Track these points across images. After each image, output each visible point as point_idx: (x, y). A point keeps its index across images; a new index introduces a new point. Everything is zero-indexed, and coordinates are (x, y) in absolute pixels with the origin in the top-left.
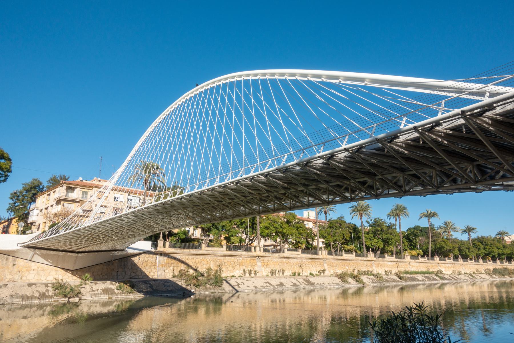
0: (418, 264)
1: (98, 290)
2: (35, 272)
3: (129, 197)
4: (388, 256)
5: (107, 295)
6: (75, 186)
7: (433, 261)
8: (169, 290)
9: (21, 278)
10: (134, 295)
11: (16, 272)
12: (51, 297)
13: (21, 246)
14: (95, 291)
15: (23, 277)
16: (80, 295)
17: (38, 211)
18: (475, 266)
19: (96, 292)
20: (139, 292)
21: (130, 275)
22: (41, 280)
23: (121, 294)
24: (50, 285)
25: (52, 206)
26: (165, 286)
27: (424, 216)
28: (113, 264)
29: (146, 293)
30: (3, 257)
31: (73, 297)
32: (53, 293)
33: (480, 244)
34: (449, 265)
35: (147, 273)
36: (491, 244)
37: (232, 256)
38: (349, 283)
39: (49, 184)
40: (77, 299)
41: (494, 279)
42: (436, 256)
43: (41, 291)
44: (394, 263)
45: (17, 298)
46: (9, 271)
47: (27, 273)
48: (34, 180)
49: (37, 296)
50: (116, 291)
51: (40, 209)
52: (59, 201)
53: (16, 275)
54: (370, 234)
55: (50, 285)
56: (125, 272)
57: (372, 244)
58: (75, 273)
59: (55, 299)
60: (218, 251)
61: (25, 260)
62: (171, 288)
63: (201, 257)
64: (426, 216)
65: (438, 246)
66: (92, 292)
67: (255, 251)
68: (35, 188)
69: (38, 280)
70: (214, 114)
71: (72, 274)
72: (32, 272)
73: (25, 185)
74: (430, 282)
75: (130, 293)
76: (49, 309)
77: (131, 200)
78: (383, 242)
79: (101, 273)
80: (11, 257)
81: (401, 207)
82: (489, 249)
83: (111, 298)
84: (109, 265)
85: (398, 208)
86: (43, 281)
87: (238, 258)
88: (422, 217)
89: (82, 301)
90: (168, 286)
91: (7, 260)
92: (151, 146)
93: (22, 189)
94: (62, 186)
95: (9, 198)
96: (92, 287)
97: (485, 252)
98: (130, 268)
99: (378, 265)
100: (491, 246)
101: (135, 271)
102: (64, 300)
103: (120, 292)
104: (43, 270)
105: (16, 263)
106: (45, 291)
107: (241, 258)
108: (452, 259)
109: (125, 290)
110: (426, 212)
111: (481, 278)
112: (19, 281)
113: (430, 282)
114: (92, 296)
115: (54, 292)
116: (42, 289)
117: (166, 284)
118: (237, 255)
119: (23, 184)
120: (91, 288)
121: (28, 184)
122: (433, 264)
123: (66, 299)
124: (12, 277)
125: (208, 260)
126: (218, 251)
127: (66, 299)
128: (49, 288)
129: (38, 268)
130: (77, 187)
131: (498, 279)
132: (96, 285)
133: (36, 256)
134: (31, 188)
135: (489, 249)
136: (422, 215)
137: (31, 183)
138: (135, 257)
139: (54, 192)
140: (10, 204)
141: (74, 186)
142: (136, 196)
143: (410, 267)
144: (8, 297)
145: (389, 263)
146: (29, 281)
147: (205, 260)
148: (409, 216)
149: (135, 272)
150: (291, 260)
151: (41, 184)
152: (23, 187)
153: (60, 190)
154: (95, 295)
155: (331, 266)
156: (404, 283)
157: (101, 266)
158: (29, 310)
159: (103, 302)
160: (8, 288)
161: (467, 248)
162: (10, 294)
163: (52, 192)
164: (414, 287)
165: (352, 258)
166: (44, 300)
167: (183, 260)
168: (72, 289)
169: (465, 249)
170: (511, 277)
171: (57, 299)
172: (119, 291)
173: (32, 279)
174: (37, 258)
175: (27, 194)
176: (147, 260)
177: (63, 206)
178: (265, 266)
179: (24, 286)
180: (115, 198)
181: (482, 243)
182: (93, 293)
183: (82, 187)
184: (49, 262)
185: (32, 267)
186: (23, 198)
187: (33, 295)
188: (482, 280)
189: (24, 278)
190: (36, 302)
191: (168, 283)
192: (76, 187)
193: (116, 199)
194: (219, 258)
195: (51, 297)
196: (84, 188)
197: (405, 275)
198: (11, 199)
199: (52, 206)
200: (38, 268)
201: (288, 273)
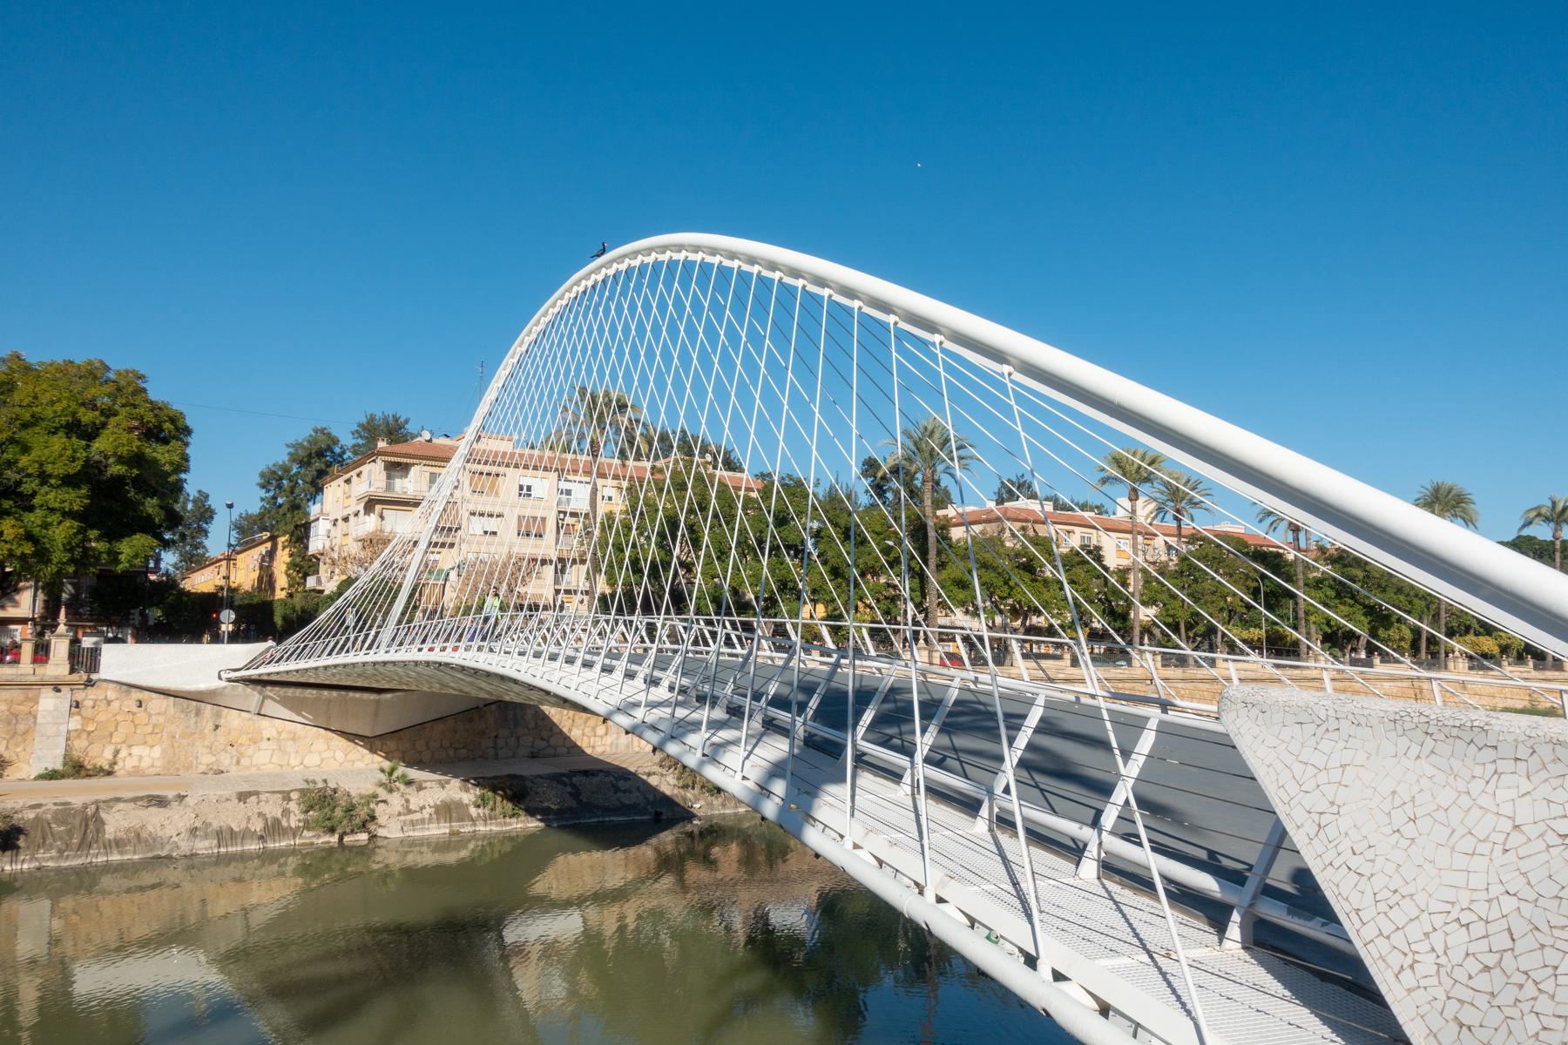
1: (422, 808)
2: (272, 745)
3: (564, 485)
4: (1382, 662)
5: (448, 825)
6: (408, 461)
7: (1557, 673)
8: (628, 806)
9: (238, 762)
10: (522, 822)
11: (222, 747)
12: (295, 832)
13: (229, 680)
14: (416, 812)
15: (242, 761)
16: (372, 827)
17: (328, 525)
19: (417, 816)
21: (532, 746)
22: (288, 764)
23: (485, 820)
24: (295, 796)
25: (356, 515)
26: (617, 790)
27: (1537, 520)
28: (481, 717)
30: (188, 707)
31: (352, 832)
32: (300, 821)
39: (360, 441)
40: (363, 837)
43: (268, 816)
44: (1406, 684)
45: (206, 837)
46: (207, 743)
47: (253, 747)
48: (316, 431)
49: (258, 830)
50: (473, 811)
51: (332, 518)
52: (371, 504)
53: (223, 753)
54: (1325, 589)
55: (295, 796)
56: (518, 739)
58: (378, 743)
59: (305, 838)
61: (243, 713)
62: (635, 797)
64: (1547, 519)
66: (405, 815)
68: (320, 454)
69: (282, 766)
70: (620, 353)
72: (264, 745)
73: (294, 446)
75: (512, 816)
76: (292, 862)
77: (568, 492)
78: (1371, 615)
79: (451, 744)
80: (209, 706)
81: (1449, 492)
83: (458, 833)
84: (471, 721)
85: (1437, 498)
86: (293, 767)
88: (1530, 523)
89: (380, 842)
90: (625, 792)
91: (197, 714)
92: (528, 393)
93: (286, 458)
94: (374, 461)
95: (258, 484)
96: (407, 801)
98: (532, 726)
101: (545, 734)
102: (328, 842)
103: (484, 814)
104: (293, 739)
105: (222, 721)
106: (279, 816)
109: (499, 810)
110: (1550, 504)
112: (234, 768)
114: (405, 828)
115: (302, 817)
116: (273, 809)
117: (622, 784)
119: (287, 446)
120: (403, 802)
121: (301, 445)
123: (334, 839)
124: (214, 759)
127: (334, 839)
128: (293, 806)
129: (280, 733)
130: (415, 461)
132: (421, 793)
133: (268, 702)
134: (310, 455)
136: (1534, 513)
137: (309, 442)
139: (358, 475)
140: (262, 500)
141: (405, 460)
142: (578, 478)
144: (183, 835)
146: (258, 769)
148: (1477, 525)
149: (545, 737)
151: (336, 441)
152: (290, 454)
153: (370, 471)
154: (413, 823)
157: (451, 721)
158: (241, 866)
159: (437, 843)
160: (186, 806)
162: (188, 826)
163: (354, 473)
166: (274, 841)
168: (350, 809)
171: (311, 837)
172: (480, 811)
173: (265, 765)
174: (271, 707)
175: (303, 471)
177: (382, 517)
179: (227, 800)
180: (521, 488)
182: (409, 817)
183: (427, 462)
185: (264, 732)
186: (292, 484)
187: (247, 827)
189: (245, 762)
190: (253, 846)
191: (626, 779)
192: (412, 461)
193: (525, 491)
195: (295, 832)
196: (434, 463)
198: (263, 487)
199: (356, 515)
200: (280, 733)
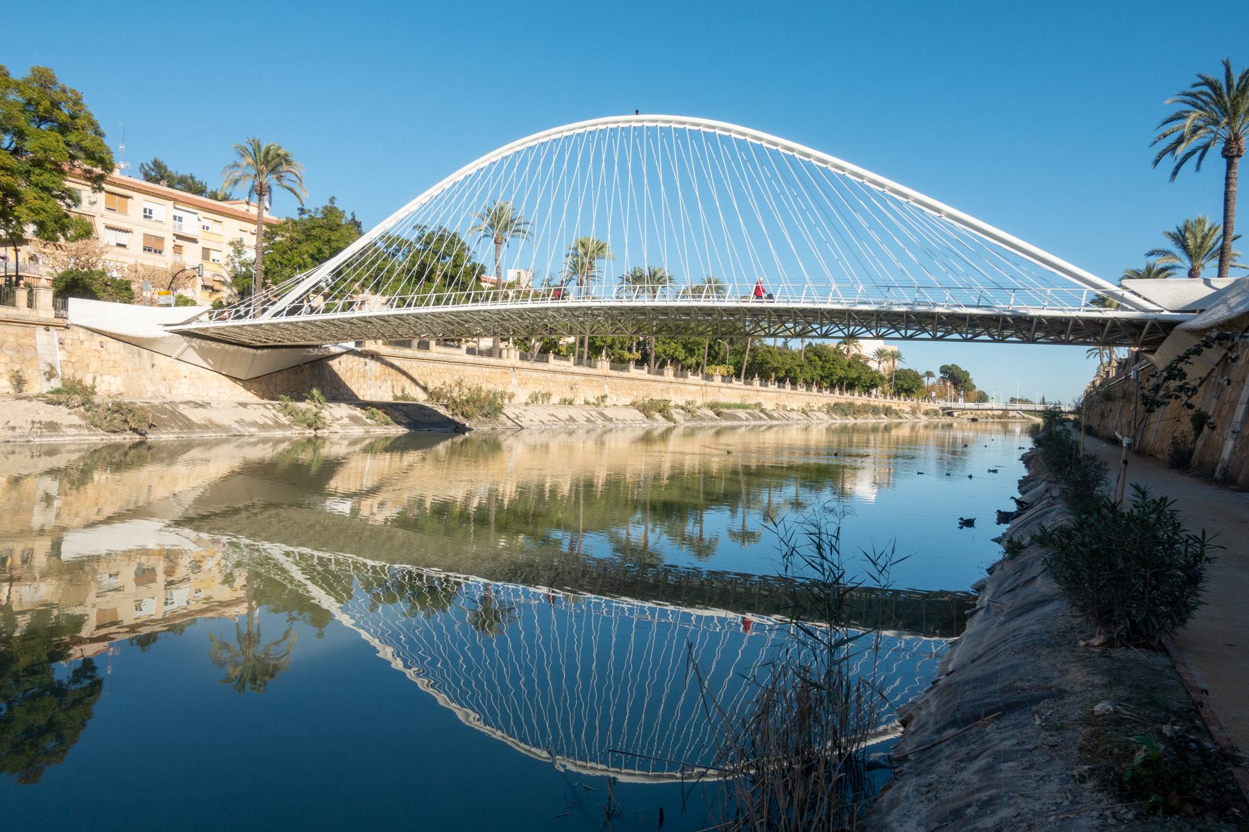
0: (730, 391)
9: (170, 392)
18: (803, 397)
20: (399, 423)
29: (407, 425)
33: (817, 358)
34: (772, 394)
35: (355, 391)
36: (834, 361)
37: (748, 390)
38: (657, 420)
41: (834, 421)
42: (604, 358)
44: (699, 388)
46: (149, 377)
57: (665, 351)
60: (450, 354)
63: (431, 365)
65: (759, 359)
67: (31, 304)
71: (245, 388)
74: (756, 423)
82: (830, 368)
87: (484, 369)
97: (821, 373)
99: (676, 391)
100: (833, 364)
101: (337, 386)
105: (155, 362)
107: (487, 370)
108: (572, 359)
111: (818, 419)
113: (756, 423)
118: (483, 363)
122: (750, 392)
125: (441, 371)
126: (450, 354)
131: (838, 421)
135: (830, 368)
138: (333, 359)
143: (720, 395)
145: (692, 388)
147: (436, 370)
150: (560, 377)
155: (523, 383)
156: (724, 423)
161: (798, 366)
164: (733, 428)
165: (642, 377)
167: (405, 369)
169: (796, 367)
170: (855, 418)
174: (193, 356)
176: (351, 366)
178: (522, 386)
181: (820, 357)
184: (208, 363)
188: (818, 421)
194: (457, 367)
197: (725, 410)
201: (555, 399)
